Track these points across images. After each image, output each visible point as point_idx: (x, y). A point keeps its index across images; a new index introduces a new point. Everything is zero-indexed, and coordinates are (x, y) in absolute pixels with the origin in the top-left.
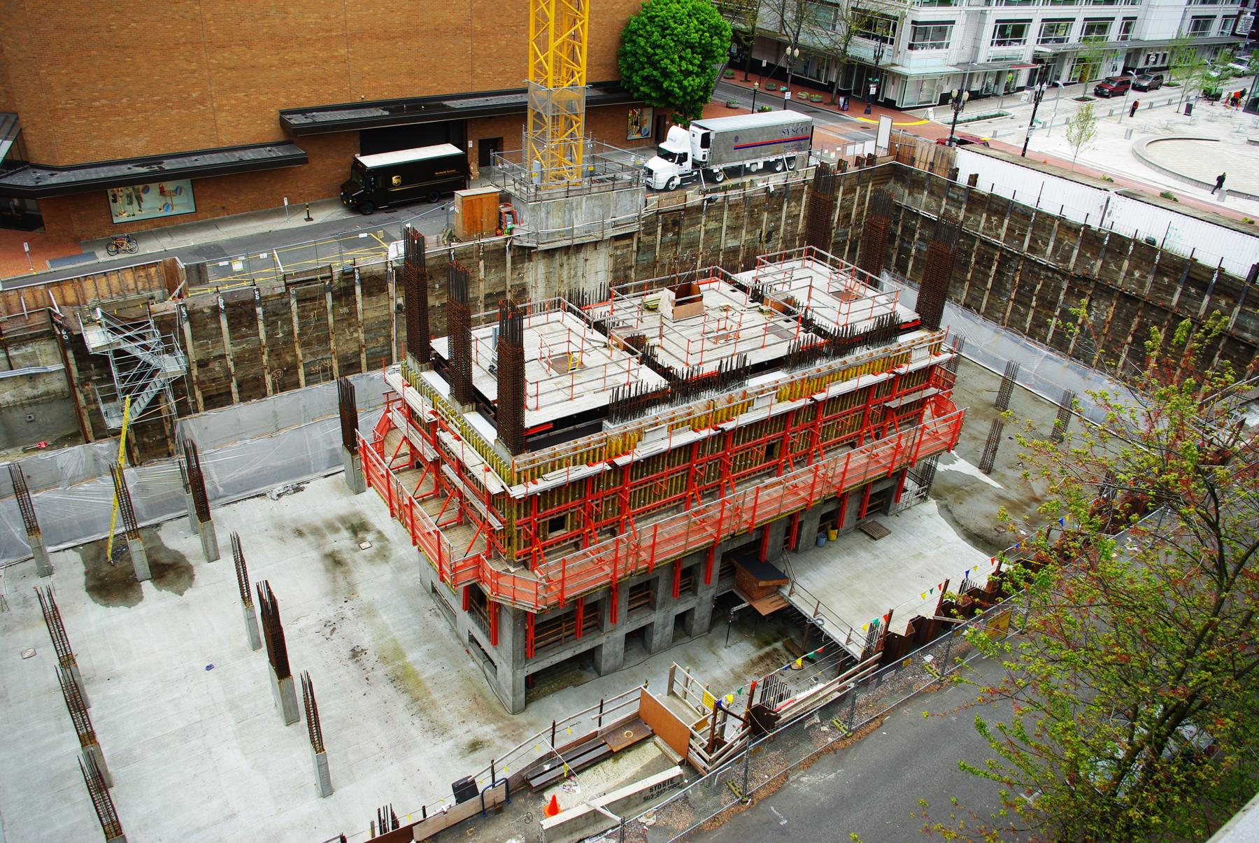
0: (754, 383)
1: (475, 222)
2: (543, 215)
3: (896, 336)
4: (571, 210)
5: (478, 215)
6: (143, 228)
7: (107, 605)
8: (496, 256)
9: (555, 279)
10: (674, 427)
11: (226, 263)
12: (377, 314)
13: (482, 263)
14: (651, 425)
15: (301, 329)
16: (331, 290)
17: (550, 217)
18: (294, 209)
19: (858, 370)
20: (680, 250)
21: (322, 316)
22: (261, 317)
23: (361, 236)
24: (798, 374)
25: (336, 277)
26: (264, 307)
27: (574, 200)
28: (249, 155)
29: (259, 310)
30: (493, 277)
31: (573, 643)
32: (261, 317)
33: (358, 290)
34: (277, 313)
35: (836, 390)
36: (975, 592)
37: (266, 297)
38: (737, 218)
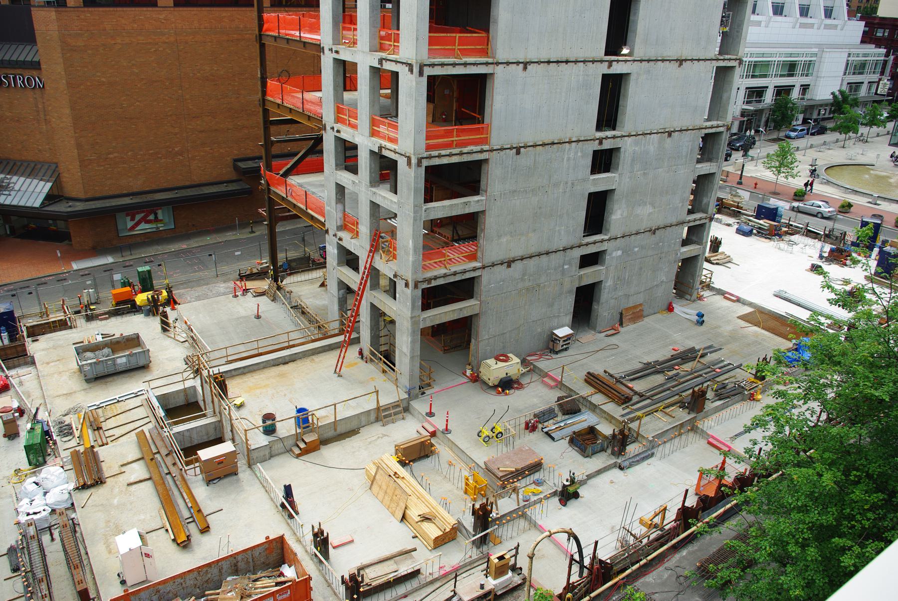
24: (150, 441)
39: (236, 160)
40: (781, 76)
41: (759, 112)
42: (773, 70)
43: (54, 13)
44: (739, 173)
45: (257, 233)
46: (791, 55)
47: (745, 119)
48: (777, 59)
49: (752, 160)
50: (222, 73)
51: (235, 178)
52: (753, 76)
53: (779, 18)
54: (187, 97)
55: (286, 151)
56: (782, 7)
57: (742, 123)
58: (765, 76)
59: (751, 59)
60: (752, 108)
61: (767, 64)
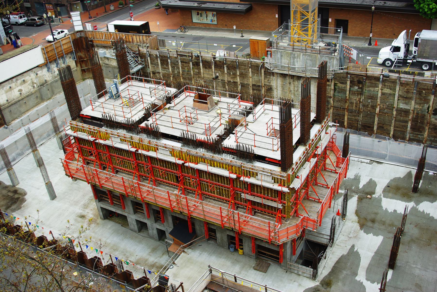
0: (164, 142)
1: (256, 52)
2: (279, 56)
3: (254, 160)
4: (294, 58)
5: (257, 49)
6: (201, 26)
7: (432, 202)
8: (256, 68)
9: (286, 89)
10: (123, 140)
11: (171, 42)
12: (208, 76)
13: (250, 70)
14: (163, 147)
15: (182, 72)
16: (192, 61)
17: (283, 58)
18: (237, 31)
19: (221, 165)
20: (363, 98)
21: (189, 70)
22: (170, 63)
23: (216, 45)
24: (185, 149)
25: (194, 57)
26: (171, 60)
27: (296, 54)
28: (230, 7)
29: (169, 60)
30: (256, 78)
31: (117, 208)
32: (170, 63)
33: (201, 64)
34: (175, 65)
35: (201, 167)
36: (72, 249)
37: (171, 57)
38: (408, 92)
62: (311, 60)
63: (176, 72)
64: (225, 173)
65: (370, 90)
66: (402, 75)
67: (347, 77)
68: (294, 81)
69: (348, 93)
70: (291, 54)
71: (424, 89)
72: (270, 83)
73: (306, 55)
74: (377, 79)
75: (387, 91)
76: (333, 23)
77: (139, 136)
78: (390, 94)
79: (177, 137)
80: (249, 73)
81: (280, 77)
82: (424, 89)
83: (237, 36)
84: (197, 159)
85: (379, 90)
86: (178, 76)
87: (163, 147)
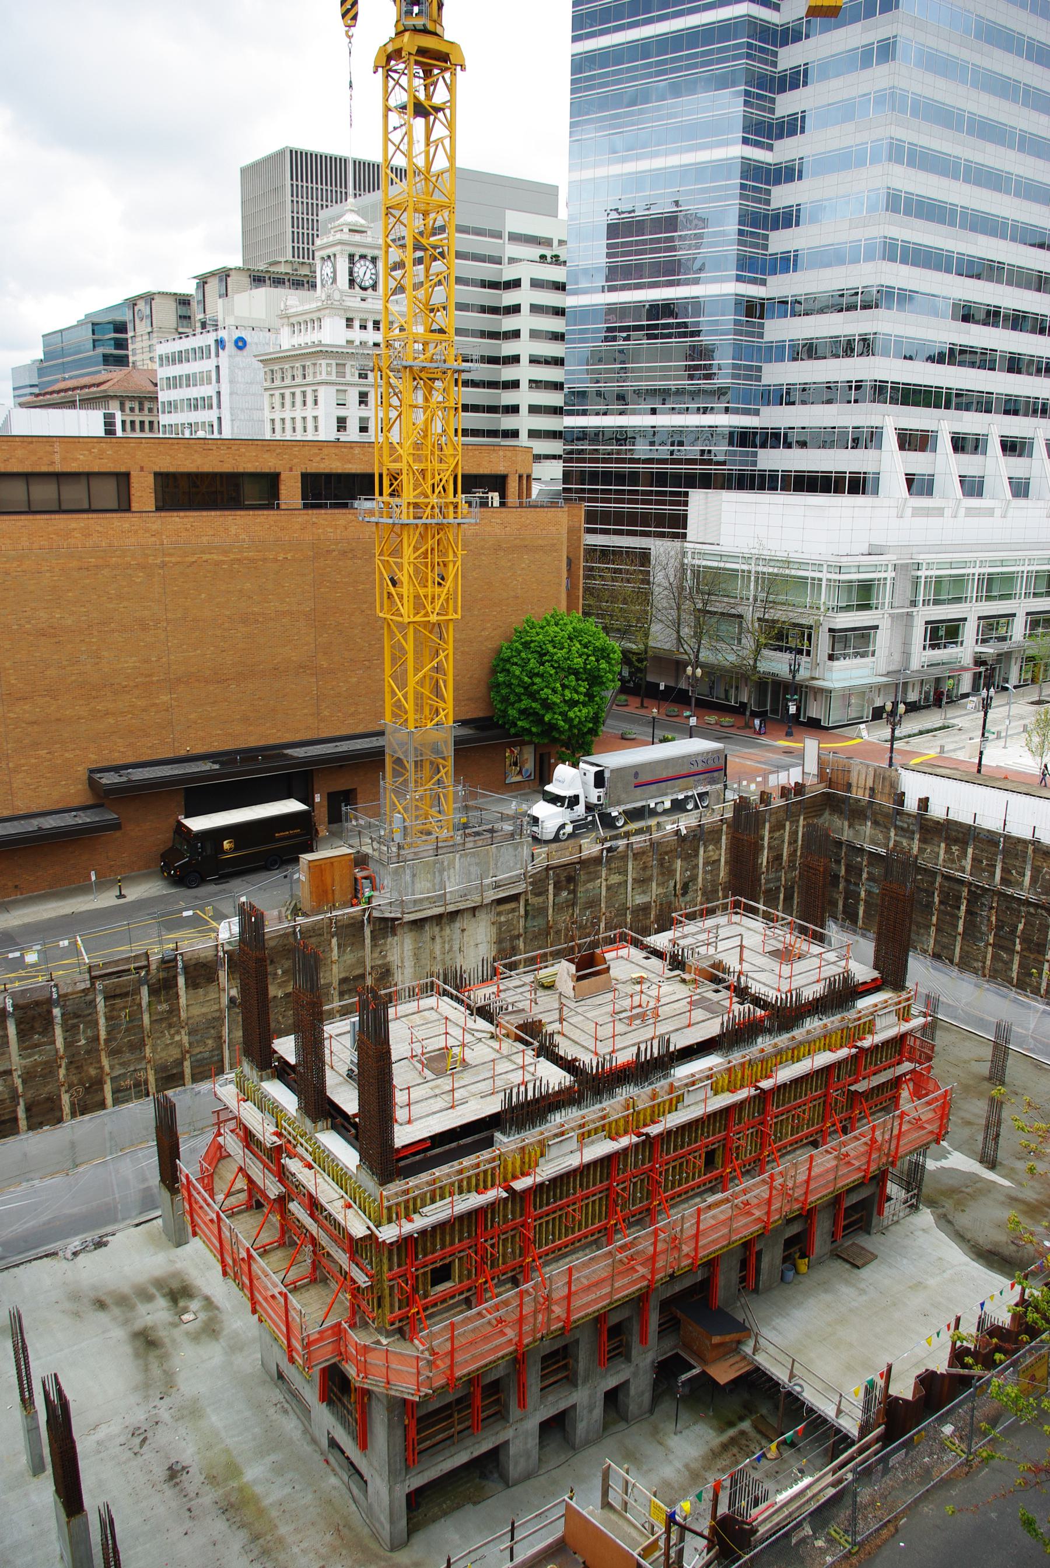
0: (682, 1072)
4: (441, 871)
5: (329, 881)
10: (585, 1136)
12: (204, 1010)
13: (334, 941)
15: (108, 1033)
16: (147, 982)
18: (102, 885)
19: (810, 1047)
21: (135, 1017)
23: (185, 914)
24: (737, 1057)
25: (153, 967)
27: (446, 858)
28: (49, 823)
29: (57, 1012)
30: (349, 958)
35: (786, 1074)
36: (996, 1331)
39: (92, 771)
40: (848, 608)
41: (1004, 658)
42: (1020, 588)
43: (565, 515)
44: (977, 761)
45: (130, 898)
46: (951, 565)
47: (982, 669)
48: (977, 571)
49: (998, 737)
50: (69, 622)
51: (90, 802)
52: (989, 598)
53: (1021, 502)
54: (7, 664)
55: (183, 753)
56: (981, 484)
57: (977, 677)
58: (958, 600)
59: (1030, 568)
60: (991, 651)
61: (1008, 579)
62: (477, 864)
63: (83, 1042)
64: (824, 1059)
65: (587, 891)
66: (633, 839)
67: (547, 877)
68: (441, 930)
69: (550, 911)
70: (435, 863)
71: (666, 853)
72: (385, 956)
73: (466, 855)
74: (597, 860)
75: (615, 879)
76: (326, 803)
77: (619, 1098)
78: (620, 884)
79: (712, 1039)
80: (331, 950)
81: (411, 930)
82: (666, 853)
83: (107, 899)
84: (766, 1065)
85: (603, 882)
86: (88, 1052)
87: (556, 1135)
